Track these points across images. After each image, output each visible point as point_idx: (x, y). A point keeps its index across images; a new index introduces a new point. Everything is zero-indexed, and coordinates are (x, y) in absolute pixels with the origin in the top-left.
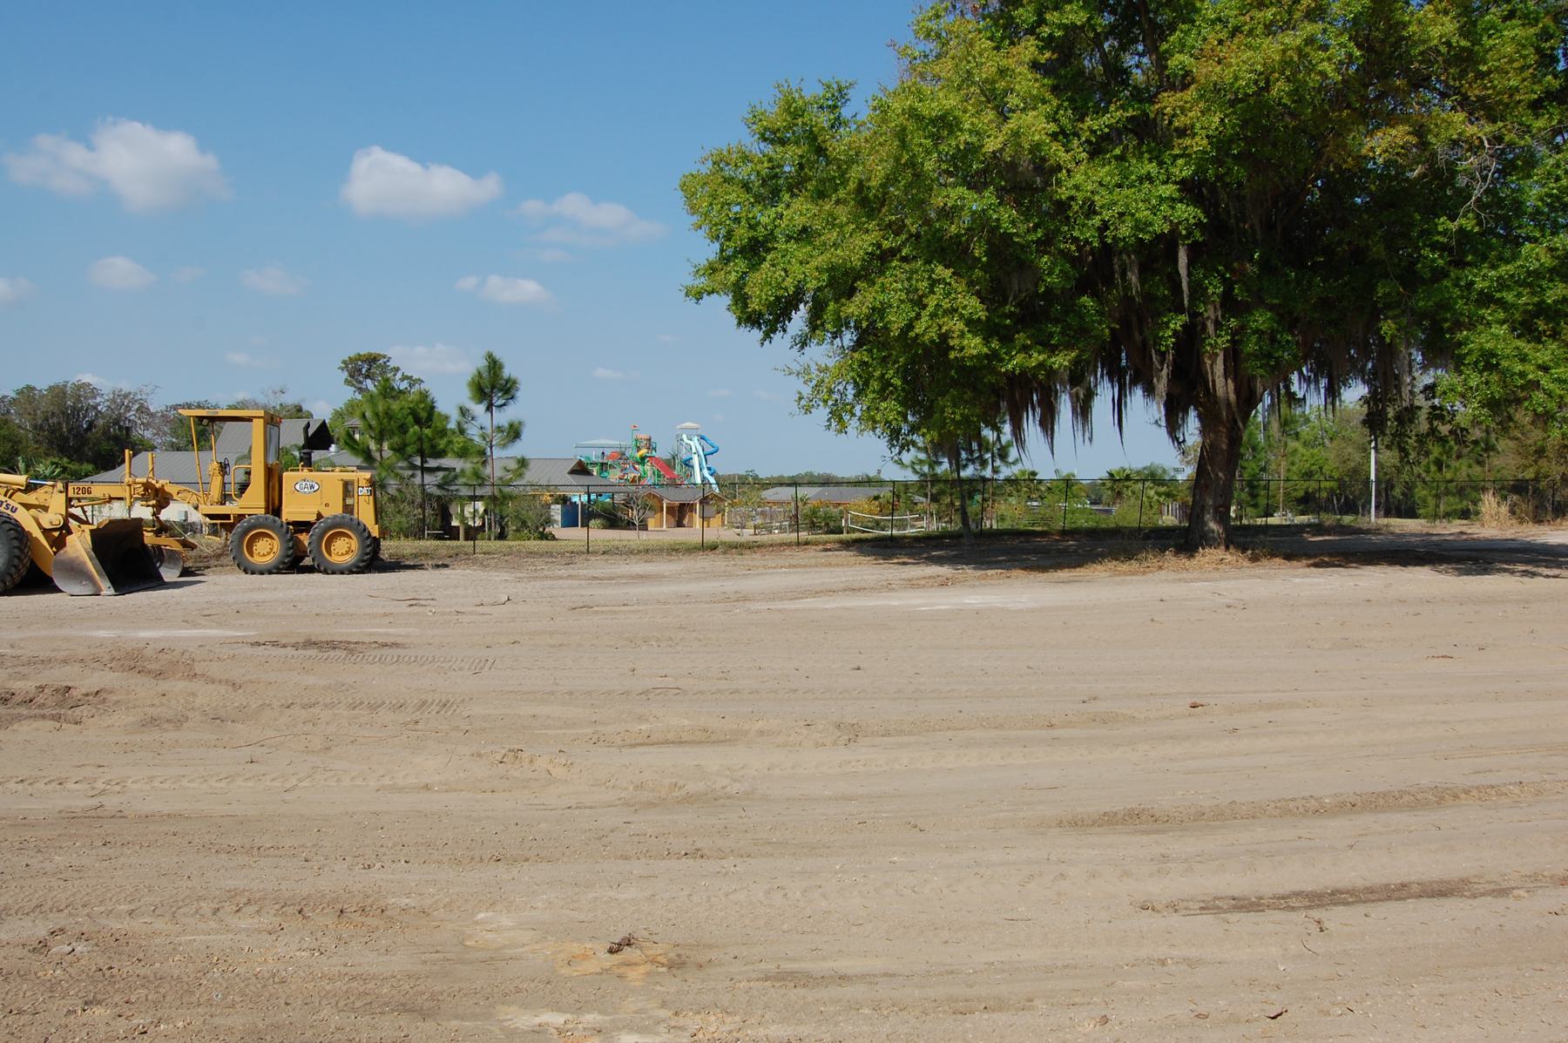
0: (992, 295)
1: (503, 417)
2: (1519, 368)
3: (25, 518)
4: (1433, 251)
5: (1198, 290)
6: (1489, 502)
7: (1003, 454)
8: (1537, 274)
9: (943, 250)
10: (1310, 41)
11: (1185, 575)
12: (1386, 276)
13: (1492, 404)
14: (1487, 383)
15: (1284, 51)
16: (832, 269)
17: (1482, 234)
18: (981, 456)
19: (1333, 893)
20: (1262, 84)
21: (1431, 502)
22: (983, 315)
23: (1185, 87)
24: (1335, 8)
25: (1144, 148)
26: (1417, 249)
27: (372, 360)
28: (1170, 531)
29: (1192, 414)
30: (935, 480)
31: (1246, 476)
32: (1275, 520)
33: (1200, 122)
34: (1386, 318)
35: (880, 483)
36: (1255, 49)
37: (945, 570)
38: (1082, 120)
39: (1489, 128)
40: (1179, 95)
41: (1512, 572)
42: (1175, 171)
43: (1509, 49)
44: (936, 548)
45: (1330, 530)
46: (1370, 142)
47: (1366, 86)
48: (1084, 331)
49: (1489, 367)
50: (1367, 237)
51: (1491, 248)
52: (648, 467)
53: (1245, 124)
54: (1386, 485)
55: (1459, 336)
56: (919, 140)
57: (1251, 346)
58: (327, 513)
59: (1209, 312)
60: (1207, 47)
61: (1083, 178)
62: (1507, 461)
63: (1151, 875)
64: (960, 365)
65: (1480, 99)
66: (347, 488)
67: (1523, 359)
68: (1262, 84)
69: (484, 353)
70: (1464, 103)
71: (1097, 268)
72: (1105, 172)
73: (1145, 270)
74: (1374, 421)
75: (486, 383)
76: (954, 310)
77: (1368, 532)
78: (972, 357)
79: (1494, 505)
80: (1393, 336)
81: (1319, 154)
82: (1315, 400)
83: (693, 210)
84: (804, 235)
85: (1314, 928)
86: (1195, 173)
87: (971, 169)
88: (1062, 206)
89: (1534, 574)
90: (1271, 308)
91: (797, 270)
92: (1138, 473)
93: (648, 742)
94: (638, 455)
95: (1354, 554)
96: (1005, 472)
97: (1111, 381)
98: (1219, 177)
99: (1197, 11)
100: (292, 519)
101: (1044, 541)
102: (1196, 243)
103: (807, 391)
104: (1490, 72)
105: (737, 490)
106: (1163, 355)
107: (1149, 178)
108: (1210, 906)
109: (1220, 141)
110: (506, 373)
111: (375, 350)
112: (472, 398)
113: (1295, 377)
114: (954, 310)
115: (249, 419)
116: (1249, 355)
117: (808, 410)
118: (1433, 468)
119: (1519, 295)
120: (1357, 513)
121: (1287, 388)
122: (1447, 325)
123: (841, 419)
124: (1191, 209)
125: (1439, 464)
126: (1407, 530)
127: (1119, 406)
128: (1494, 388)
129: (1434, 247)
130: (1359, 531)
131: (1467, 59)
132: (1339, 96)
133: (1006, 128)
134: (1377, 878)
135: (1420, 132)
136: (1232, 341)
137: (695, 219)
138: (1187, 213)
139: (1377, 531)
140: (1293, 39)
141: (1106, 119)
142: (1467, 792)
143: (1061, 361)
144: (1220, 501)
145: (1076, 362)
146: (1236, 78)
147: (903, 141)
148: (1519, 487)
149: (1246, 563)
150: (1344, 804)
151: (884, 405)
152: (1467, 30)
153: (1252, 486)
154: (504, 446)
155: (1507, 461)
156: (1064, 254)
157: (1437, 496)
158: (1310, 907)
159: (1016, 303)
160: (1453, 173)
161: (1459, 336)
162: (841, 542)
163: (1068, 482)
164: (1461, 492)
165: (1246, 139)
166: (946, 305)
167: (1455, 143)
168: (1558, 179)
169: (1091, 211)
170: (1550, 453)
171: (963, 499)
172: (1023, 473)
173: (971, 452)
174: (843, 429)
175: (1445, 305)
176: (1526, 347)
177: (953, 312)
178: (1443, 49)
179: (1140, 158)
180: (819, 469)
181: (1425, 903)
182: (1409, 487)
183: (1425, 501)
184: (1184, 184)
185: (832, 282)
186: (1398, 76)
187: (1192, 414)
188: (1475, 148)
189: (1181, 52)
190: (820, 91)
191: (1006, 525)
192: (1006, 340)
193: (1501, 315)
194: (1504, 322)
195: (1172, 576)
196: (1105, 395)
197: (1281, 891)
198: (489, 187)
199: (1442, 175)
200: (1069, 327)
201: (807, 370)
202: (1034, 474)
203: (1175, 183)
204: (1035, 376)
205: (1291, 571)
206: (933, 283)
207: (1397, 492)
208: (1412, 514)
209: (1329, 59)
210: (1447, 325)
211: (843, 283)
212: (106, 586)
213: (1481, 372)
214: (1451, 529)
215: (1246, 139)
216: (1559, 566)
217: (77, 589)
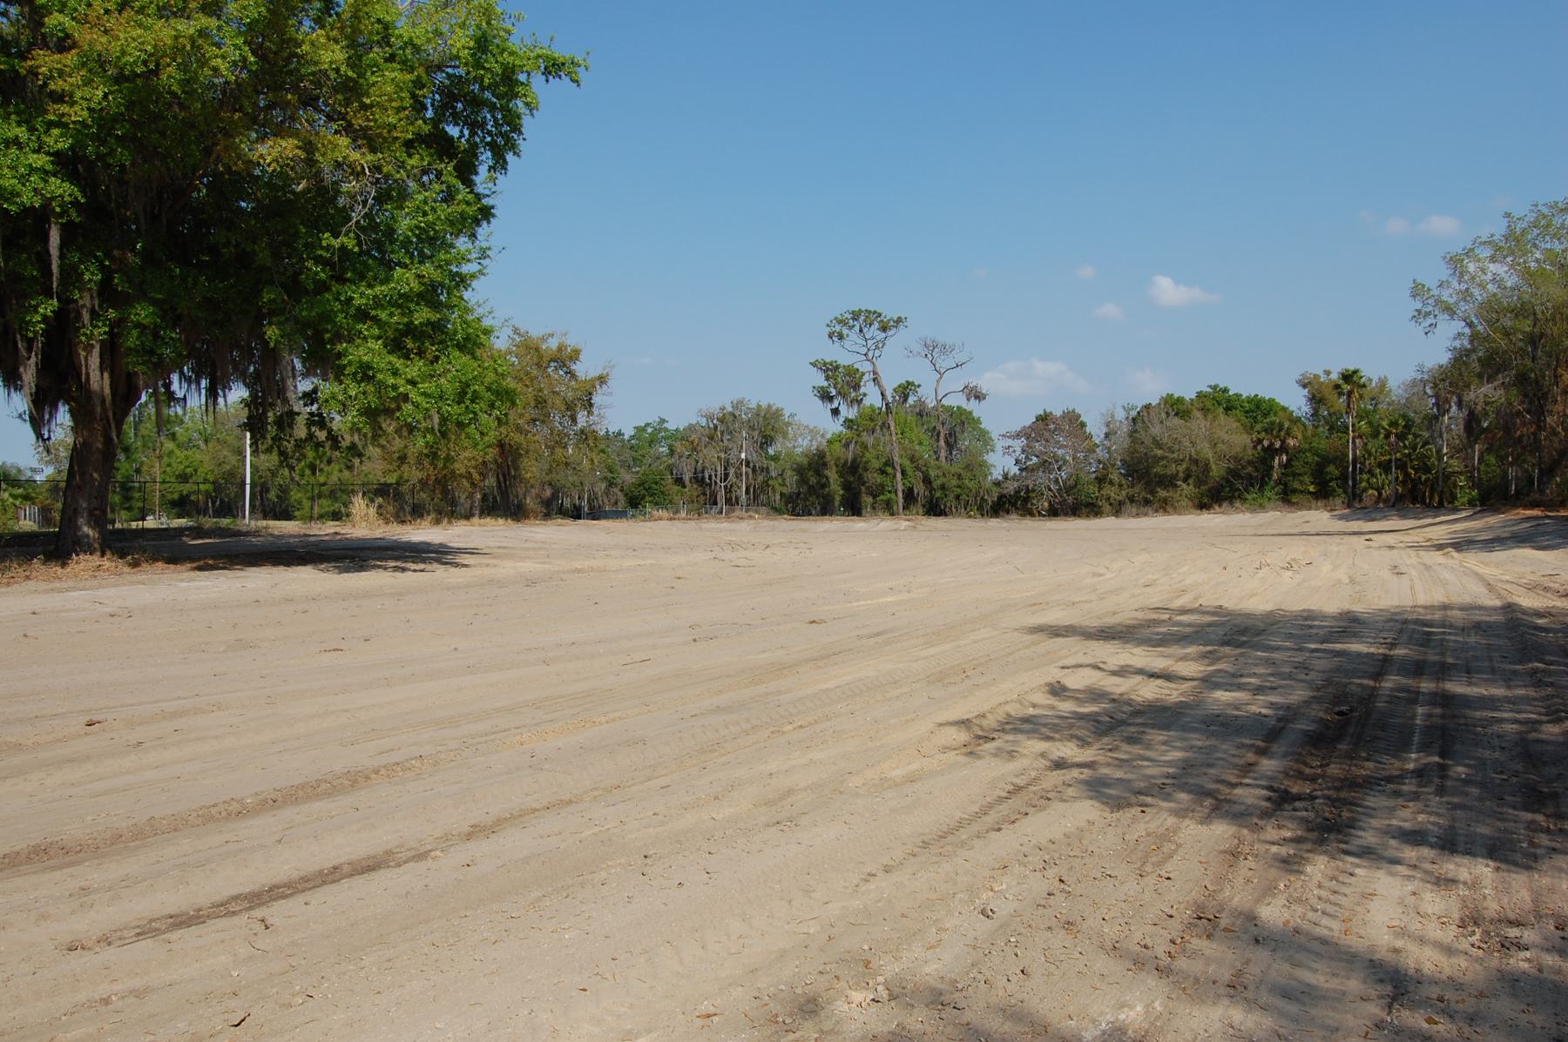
2: (391, 381)
4: (316, 264)
5: (71, 276)
6: (359, 505)
10: (203, 33)
11: (57, 584)
12: (272, 283)
13: (370, 413)
14: (364, 393)
15: (176, 38)
17: (361, 253)
19: (270, 890)
20: (152, 66)
21: (307, 504)
24: (232, 8)
25: (12, 109)
26: (302, 260)
32: (150, 523)
34: (270, 324)
36: (146, 28)
39: (370, 157)
40: (57, 57)
42: (49, 141)
43: (389, 89)
45: (210, 532)
46: (262, 149)
47: (259, 93)
49: (368, 378)
50: (254, 242)
51: (368, 268)
53: (130, 105)
54: (261, 489)
57: (132, 340)
59: (85, 300)
60: (92, 15)
62: (375, 467)
63: (73, 912)
65: (364, 129)
67: (395, 373)
68: (152, 66)
70: (348, 129)
74: (255, 424)
77: (247, 534)
79: (363, 506)
80: (277, 342)
81: (208, 152)
82: (197, 401)
85: (259, 927)
86: (72, 148)
89: (404, 570)
90: (154, 302)
95: (237, 556)
98: (100, 157)
102: (71, 223)
104: (371, 106)
106: (30, 343)
107: (16, 142)
108: (147, 930)
109: (101, 118)
113: (175, 378)
116: (130, 349)
118: (308, 472)
119: (391, 315)
120: (235, 517)
121: (168, 386)
122: (327, 336)
124: (66, 185)
125: (313, 468)
126: (286, 531)
128: (370, 398)
129: (318, 260)
130: (239, 534)
131: (351, 90)
132: (232, 96)
134: (310, 867)
135: (309, 147)
136: (110, 333)
138: (61, 188)
139: (256, 533)
140: (187, 28)
142: (376, 772)
146: (124, 53)
148: (382, 491)
149: (127, 569)
150: (265, 801)
152: (353, 62)
153: (126, 489)
155: (375, 467)
157: (312, 499)
158: (251, 908)
160: (338, 192)
164: (332, 495)
165: (131, 121)
167: (338, 165)
168: (425, 214)
170: (412, 460)
175: (327, 317)
176: (399, 363)
178: (333, 75)
181: (359, 880)
182: (284, 490)
183: (300, 503)
184: (57, 156)
186: (287, 90)
188: (358, 174)
189: (61, 12)
194: (379, 338)
195: (43, 586)
197: (217, 899)
199: (325, 194)
203: (48, 154)
205: (175, 576)
207: (272, 495)
208: (287, 516)
209: (223, 57)
210: (327, 336)
213: (359, 383)
214: (326, 530)
215: (131, 121)
216: (424, 561)
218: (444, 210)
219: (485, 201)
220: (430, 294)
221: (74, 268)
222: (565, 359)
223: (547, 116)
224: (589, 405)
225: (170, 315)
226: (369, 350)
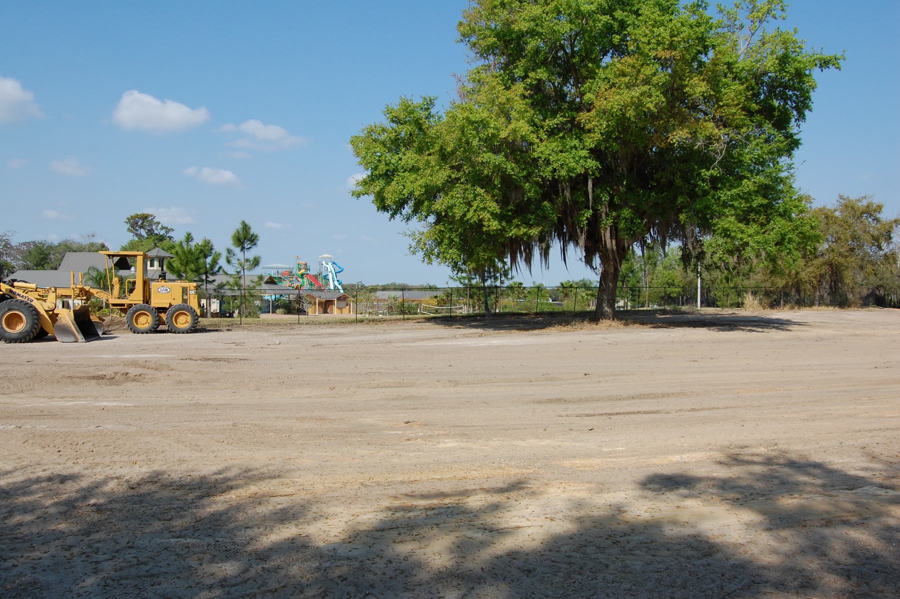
0: (503, 202)
1: (251, 254)
2: (740, 236)
3: (37, 304)
6: (749, 299)
7: (506, 274)
8: (749, 193)
9: (480, 180)
16: (426, 186)
18: (494, 275)
22: (498, 211)
23: (589, 110)
27: (145, 217)
28: (590, 312)
29: (598, 255)
30: (471, 287)
31: (630, 286)
33: (596, 125)
35: (436, 289)
37: (480, 331)
38: (544, 120)
41: (743, 330)
44: (473, 321)
45: (671, 311)
48: (545, 218)
52: (305, 280)
55: (714, 221)
56: (470, 131)
57: (622, 225)
58: (174, 303)
59: (603, 209)
61: (544, 148)
64: (488, 233)
66: (185, 291)
67: (742, 232)
69: (240, 221)
71: (551, 188)
72: (554, 145)
73: (573, 189)
74: (686, 258)
75: (242, 236)
76: (485, 208)
78: (493, 230)
83: (358, 154)
84: (414, 169)
87: (494, 145)
88: (535, 160)
90: (631, 207)
91: (410, 187)
92: (577, 284)
93: (378, 386)
94: (300, 273)
96: (507, 283)
97: (559, 239)
98: (606, 148)
99: (596, 73)
100: (157, 306)
101: (527, 318)
102: (596, 177)
103: (414, 244)
104: (722, 106)
105: (352, 294)
106: (582, 229)
110: (252, 231)
111: (146, 211)
112: (234, 244)
114: (485, 208)
115: (136, 256)
117: (414, 253)
118: (724, 281)
123: (429, 258)
127: (564, 251)
129: (703, 180)
133: (509, 127)
135: (694, 134)
137: (359, 159)
138: (592, 164)
140: (636, 92)
141: (556, 121)
143: (535, 232)
144: (610, 297)
145: (541, 232)
146: (612, 108)
147: (463, 132)
149: (622, 326)
151: (451, 251)
154: (250, 269)
156: (537, 183)
159: (514, 206)
161: (714, 221)
162: (425, 318)
163: (539, 288)
166: (482, 206)
169: (548, 162)
171: (486, 297)
172: (515, 283)
173: (490, 273)
174: (430, 263)
175: (707, 207)
177: (485, 209)
179: (571, 138)
180: (399, 281)
184: (592, 151)
185: (426, 192)
187: (598, 255)
190: (420, 101)
191: (507, 310)
192: (509, 222)
193: (733, 212)
196: (556, 246)
198: (200, 115)
200: (538, 216)
201: (414, 234)
202: (521, 284)
204: (522, 239)
206: (475, 196)
211: (431, 193)
212: (80, 337)
217: (66, 339)
218: (766, 148)
219: (795, 137)
220: (765, 190)
221: (598, 196)
222: (871, 211)
223: (824, 87)
224: (889, 238)
225: (639, 212)
226: (729, 222)
